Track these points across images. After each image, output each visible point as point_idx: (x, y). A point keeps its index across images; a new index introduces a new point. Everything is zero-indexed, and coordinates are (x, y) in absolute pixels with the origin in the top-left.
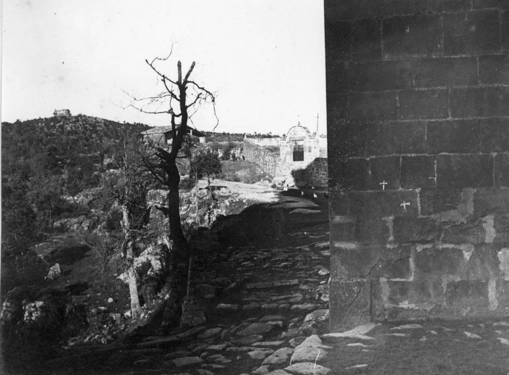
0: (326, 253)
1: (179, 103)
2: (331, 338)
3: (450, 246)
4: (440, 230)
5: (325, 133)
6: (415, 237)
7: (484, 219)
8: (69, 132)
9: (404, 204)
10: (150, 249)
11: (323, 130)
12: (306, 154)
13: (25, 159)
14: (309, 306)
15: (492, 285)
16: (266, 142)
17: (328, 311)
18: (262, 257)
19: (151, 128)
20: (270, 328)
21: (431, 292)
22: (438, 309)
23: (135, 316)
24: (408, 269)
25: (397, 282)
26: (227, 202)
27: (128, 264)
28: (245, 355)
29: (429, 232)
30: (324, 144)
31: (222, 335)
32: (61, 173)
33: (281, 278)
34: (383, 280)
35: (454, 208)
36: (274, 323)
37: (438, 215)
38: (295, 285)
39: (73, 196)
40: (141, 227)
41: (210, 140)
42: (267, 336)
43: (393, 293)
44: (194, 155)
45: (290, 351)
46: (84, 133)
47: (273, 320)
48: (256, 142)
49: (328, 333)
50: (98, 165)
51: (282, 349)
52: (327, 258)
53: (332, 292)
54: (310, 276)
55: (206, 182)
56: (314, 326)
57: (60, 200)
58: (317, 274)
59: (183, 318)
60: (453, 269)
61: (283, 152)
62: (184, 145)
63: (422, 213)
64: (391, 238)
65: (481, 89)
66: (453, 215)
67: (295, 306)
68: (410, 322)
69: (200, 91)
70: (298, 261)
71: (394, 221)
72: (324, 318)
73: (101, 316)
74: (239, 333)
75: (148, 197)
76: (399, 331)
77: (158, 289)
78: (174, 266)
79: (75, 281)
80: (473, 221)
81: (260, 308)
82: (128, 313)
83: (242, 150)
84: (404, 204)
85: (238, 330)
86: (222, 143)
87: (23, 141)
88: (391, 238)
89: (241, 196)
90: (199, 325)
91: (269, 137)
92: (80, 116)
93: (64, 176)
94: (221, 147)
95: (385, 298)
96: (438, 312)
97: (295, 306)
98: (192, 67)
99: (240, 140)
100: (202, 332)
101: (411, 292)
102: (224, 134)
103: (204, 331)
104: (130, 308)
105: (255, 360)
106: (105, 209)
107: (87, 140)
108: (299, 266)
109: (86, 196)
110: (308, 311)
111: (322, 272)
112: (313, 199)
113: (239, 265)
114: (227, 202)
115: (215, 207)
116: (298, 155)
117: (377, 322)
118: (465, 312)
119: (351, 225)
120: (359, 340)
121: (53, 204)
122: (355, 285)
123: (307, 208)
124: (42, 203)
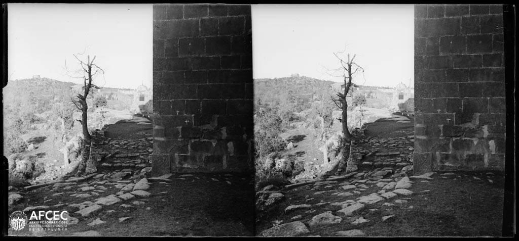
0: (412, 140)
1: (348, 72)
2: (414, 178)
3: (468, 139)
4: (464, 131)
5: (414, 87)
6: (191, 136)
7: (483, 127)
8: (39, 86)
9: (187, 121)
10: (74, 138)
11: (413, 86)
12: (404, 97)
13: (278, 95)
14: (404, 164)
15: (225, 157)
16: (128, 92)
17: (412, 166)
18: (124, 143)
19: (76, 84)
20: (126, 174)
21: (198, 160)
22: (461, 167)
23: (326, 166)
24: (449, 148)
25: (182, 156)
26: (109, 119)
27: (323, 143)
28: (375, 185)
29: (459, 132)
30: (413, 92)
31: (365, 176)
32: (294, 102)
33: (132, 153)
34: (176, 154)
35: (470, 122)
36: (388, 171)
37: (463, 125)
38: (398, 154)
39: (40, 114)
40: (70, 129)
41: (362, 89)
42: (385, 176)
43: (442, 158)
44: (354, 96)
45: (395, 183)
46: (46, 86)
47: (388, 170)
48: (382, 90)
49: (151, 177)
50: (311, 99)
51: (391, 183)
52: (413, 143)
53: (414, 158)
54: (145, 152)
55: (100, 109)
56: (406, 173)
57: (293, 114)
58: (148, 151)
59: (347, 168)
60: (469, 149)
61: (394, 96)
62: (350, 91)
63: (456, 124)
64: (442, 134)
65: (484, 69)
66: (470, 125)
67: (398, 164)
68: (188, 174)
69: (98, 69)
70: (139, 146)
71: (182, 129)
72: (150, 171)
73: (310, 166)
74: (373, 175)
75: (73, 115)
76: (443, 176)
77: (336, 155)
78: (344, 145)
79: (299, 151)
80: (478, 128)
81: (121, 166)
82: (322, 165)
83: (117, 95)
84: (448, 120)
85: (372, 174)
86: (367, 91)
87: (277, 87)
88: (180, 136)
89: (116, 116)
90: (94, 173)
91: (129, 90)
92: (44, 78)
93: (295, 104)
94: (107, 94)
95: (177, 163)
96: (461, 167)
97: (137, 165)
98: (354, 56)
99: (116, 91)
100: (355, 174)
101: (450, 159)
102: (109, 88)
103: (96, 175)
104: (64, 164)
105: (118, 189)
106: (313, 119)
107: (47, 89)
108: (140, 147)
109: (46, 114)
110: (143, 168)
111: (411, 149)
112: (407, 116)
113: (113, 146)
114: (109, 119)
115: (363, 119)
116: (401, 97)
117: (434, 171)
118: (474, 168)
119: (162, 130)
120: (426, 179)
121: (290, 116)
122: (425, 155)
123: (146, 122)
124: (26, 117)
